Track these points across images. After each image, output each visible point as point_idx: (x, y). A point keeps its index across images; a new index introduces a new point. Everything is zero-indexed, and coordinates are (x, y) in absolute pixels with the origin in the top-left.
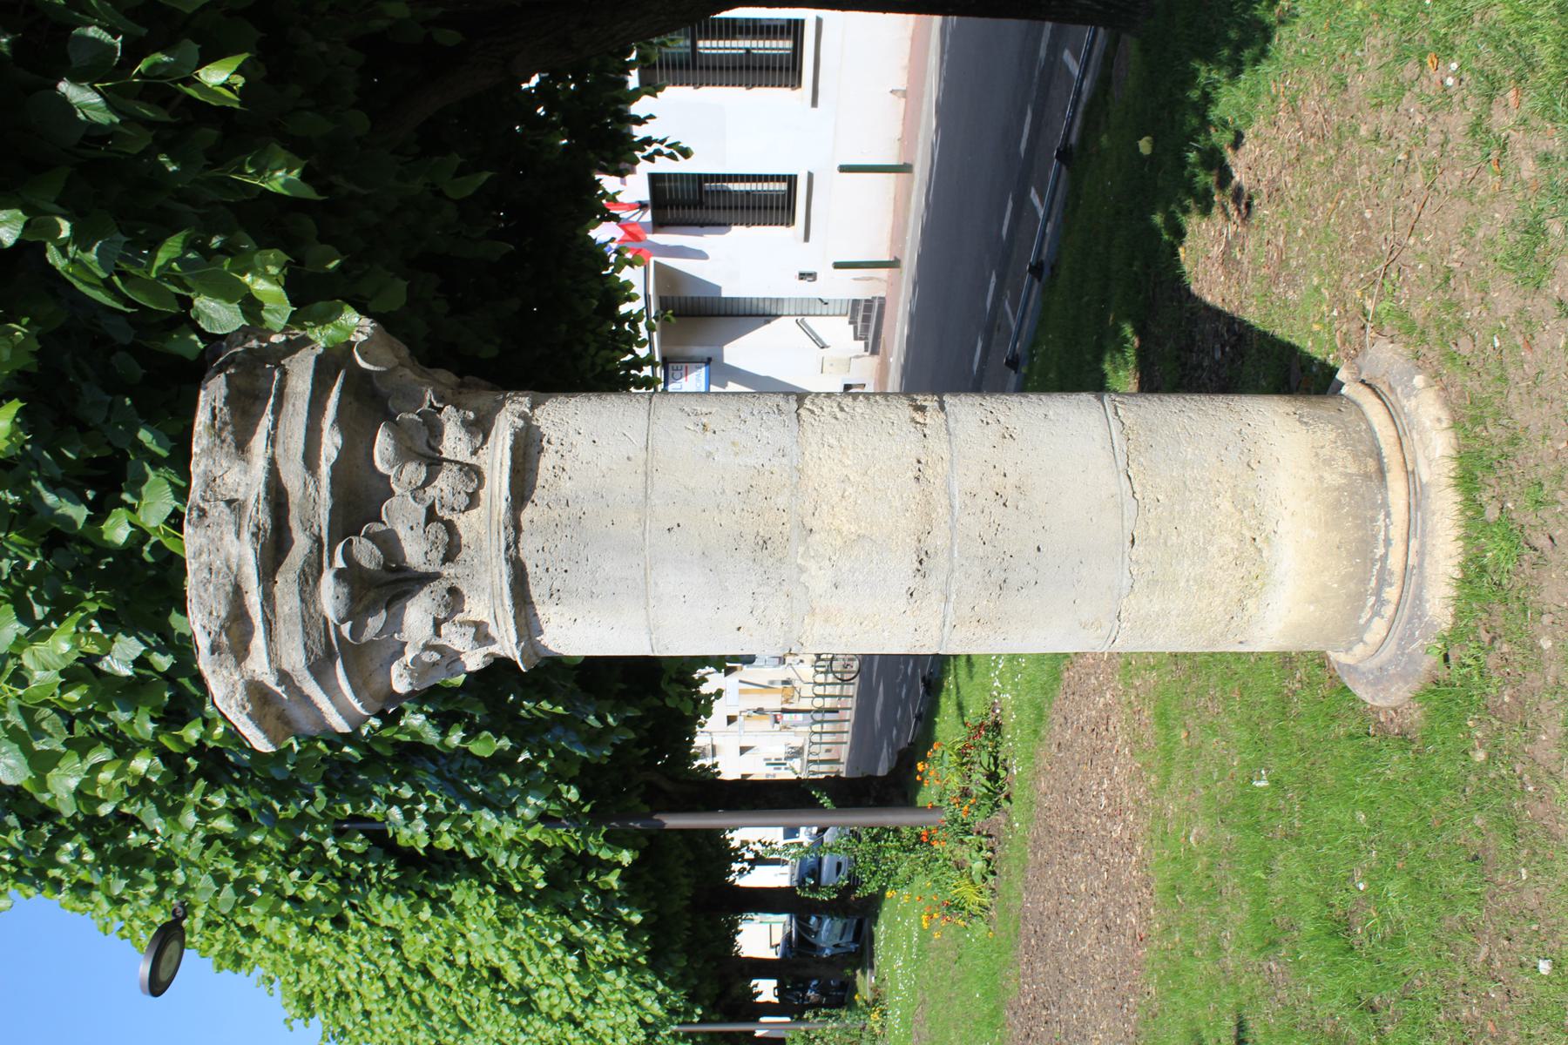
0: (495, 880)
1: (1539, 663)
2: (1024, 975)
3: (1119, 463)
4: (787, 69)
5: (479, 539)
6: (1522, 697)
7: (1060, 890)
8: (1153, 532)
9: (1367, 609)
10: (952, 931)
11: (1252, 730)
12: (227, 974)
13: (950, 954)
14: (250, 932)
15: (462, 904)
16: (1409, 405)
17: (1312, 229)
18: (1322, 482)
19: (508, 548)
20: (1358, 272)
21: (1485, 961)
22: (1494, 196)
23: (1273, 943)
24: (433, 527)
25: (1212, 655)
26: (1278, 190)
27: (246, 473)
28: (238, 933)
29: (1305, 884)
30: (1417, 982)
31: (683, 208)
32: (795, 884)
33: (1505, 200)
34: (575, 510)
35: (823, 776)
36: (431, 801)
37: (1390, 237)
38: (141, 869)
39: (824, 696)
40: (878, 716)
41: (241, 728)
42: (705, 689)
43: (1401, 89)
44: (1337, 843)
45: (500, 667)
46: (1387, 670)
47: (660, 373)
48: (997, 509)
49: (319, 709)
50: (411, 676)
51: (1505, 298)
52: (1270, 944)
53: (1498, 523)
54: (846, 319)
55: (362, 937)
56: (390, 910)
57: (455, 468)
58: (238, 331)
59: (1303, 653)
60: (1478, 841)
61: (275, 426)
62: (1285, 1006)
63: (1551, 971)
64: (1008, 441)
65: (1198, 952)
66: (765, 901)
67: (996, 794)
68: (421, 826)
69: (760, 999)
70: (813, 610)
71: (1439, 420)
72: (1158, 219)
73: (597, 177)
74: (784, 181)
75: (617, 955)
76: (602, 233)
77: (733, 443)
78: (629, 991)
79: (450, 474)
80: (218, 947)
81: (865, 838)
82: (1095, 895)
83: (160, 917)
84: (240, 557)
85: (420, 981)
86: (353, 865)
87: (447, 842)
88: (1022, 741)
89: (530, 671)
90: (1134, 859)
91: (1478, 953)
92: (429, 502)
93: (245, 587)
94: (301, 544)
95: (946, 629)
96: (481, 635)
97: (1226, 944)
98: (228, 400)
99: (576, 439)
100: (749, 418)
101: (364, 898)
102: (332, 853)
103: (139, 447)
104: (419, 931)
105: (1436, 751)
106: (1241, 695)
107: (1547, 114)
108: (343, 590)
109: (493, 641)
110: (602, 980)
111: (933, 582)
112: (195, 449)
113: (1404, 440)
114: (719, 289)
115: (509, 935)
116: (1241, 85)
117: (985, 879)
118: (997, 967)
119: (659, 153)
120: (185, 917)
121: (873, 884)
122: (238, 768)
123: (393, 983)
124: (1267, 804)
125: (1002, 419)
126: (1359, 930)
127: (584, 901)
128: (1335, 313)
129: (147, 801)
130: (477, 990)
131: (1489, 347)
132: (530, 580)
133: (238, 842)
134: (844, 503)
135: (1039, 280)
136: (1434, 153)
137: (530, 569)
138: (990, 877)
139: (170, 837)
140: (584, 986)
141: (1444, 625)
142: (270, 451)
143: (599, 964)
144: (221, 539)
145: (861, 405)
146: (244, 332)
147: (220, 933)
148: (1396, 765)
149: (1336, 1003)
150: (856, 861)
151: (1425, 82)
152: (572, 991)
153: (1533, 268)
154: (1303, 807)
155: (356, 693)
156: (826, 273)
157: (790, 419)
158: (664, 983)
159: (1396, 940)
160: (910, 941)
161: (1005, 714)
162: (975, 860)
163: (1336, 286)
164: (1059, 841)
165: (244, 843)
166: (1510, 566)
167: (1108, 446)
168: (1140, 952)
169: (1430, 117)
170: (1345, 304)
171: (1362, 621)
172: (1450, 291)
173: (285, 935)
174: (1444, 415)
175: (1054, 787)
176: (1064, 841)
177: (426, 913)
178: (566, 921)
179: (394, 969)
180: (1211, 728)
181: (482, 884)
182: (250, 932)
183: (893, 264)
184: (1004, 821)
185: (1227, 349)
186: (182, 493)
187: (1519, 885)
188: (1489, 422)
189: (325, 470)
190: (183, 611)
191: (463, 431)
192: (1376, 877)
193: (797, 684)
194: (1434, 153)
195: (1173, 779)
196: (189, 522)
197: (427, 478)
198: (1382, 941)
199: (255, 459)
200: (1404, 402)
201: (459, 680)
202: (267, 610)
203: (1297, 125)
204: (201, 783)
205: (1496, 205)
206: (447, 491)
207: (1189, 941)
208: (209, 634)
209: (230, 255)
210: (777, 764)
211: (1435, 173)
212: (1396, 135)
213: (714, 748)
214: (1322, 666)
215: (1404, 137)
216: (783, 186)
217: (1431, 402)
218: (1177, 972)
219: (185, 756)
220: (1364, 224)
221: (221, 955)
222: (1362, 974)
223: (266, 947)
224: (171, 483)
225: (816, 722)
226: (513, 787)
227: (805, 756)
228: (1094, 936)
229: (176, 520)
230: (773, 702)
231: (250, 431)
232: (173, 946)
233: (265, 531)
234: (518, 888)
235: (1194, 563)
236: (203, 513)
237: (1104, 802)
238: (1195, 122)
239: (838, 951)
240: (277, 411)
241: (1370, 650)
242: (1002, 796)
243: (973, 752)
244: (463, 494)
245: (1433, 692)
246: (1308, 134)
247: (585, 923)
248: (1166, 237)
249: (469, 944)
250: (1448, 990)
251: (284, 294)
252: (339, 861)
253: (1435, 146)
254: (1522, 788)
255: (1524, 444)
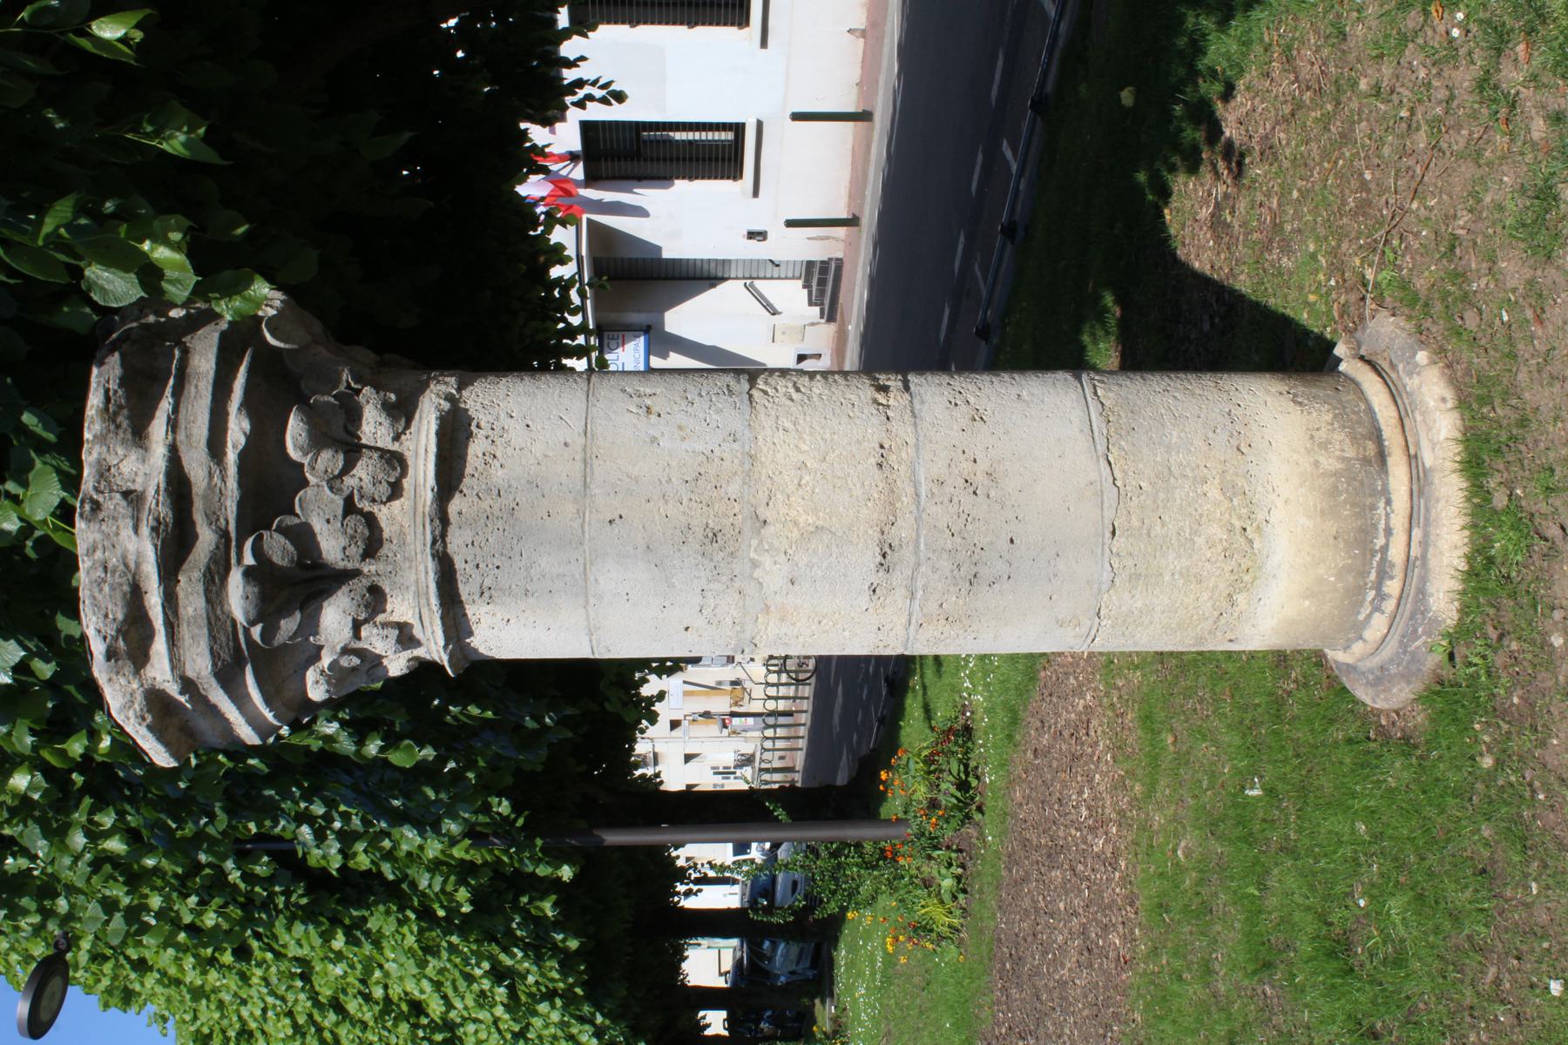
0: (416, 904)
1: (1551, 662)
2: (999, 1003)
3: (1099, 447)
4: (730, 160)
5: (402, 534)
6: (1532, 697)
7: (1037, 910)
8: (1135, 522)
9: (1367, 604)
10: (919, 956)
11: (1244, 735)
12: (115, 1012)
13: (917, 980)
14: (141, 966)
15: (379, 931)
16: (1412, 383)
17: (1308, 191)
18: (1317, 467)
19: (434, 542)
20: (1358, 238)
21: (1493, 982)
22: (1503, 158)
23: (1268, 965)
24: (352, 520)
25: (1200, 653)
26: (1271, 148)
27: (144, 461)
28: (128, 966)
29: (1300, 900)
30: (1421, 1006)
31: (619, 160)
32: (746, 905)
33: (1514, 162)
34: (507, 500)
35: (776, 786)
36: (346, 817)
37: (1391, 201)
38: (20, 898)
39: (776, 698)
40: (836, 719)
41: (140, 741)
42: (646, 691)
43: (1404, 40)
44: (1335, 857)
45: (425, 670)
46: (1388, 670)
47: (593, 340)
48: (967, 499)
49: (227, 720)
50: (328, 683)
51: (1514, 270)
52: (1264, 965)
53: (1507, 511)
54: (800, 283)
55: (267, 969)
56: (299, 939)
57: (376, 455)
58: (134, 304)
59: (1299, 652)
60: (1486, 853)
61: (176, 409)
62: (1280, 1033)
63: (1563, 992)
64: (979, 424)
65: (1185, 975)
66: (713, 924)
67: (967, 805)
68: (333, 847)
69: (708, 1032)
70: (767, 607)
71: (1444, 400)
72: (1142, 177)
73: (523, 126)
74: (730, 130)
75: (551, 985)
76: (532, 188)
77: (680, 428)
78: (563, 1025)
79: (370, 462)
80: (106, 982)
81: (824, 854)
82: (1075, 914)
83: (39, 950)
84: (139, 554)
85: (332, 1017)
86: (257, 889)
87: (363, 861)
88: (995, 747)
89: (459, 676)
90: (1117, 874)
91: (1486, 974)
92: (346, 492)
93: (144, 586)
94: (206, 538)
95: (912, 627)
96: (406, 637)
97: (1217, 967)
98: (123, 382)
99: (508, 423)
100: (697, 399)
101: (270, 925)
102: (235, 876)
103: (24, 430)
104: (331, 961)
105: (1441, 757)
106: (1232, 697)
107: (1559, 70)
108: (253, 590)
109: (418, 644)
110: (535, 1013)
111: (899, 577)
112: (87, 435)
113: (1406, 421)
114: (659, 249)
115: (431, 965)
116: (1232, 32)
117: (955, 898)
118: (969, 994)
119: (589, 97)
120: (68, 949)
121: (833, 904)
122: (130, 786)
123: (301, 1020)
124: (1261, 815)
125: (972, 400)
126: (1359, 950)
127: (514, 926)
128: (1333, 283)
129: (30, 822)
130: (396, 1025)
131: (1497, 321)
132: (459, 577)
133: (130, 866)
134: (800, 492)
135: (1012, 243)
136: (1439, 110)
137: (459, 564)
138: (961, 896)
139: (53, 860)
140: (514, 1020)
141: (1449, 622)
142: (170, 437)
143: (531, 995)
144: (117, 534)
145: (819, 385)
146: (141, 306)
147: (108, 967)
148: (1397, 772)
149: (1335, 1029)
150: (813, 880)
151: (1430, 33)
152: (502, 1026)
153: (1542, 238)
154: (1299, 817)
155: (268, 701)
156: (777, 231)
157: (742, 401)
158: (603, 1015)
159: (1399, 961)
160: (873, 967)
161: (977, 717)
162: (945, 877)
163: (1333, 253)
164: (1035, 856)
165: (136, 867)
166: (1519, 558)
167: (1087, 429)
168: (1124, 976)
169: (1434, 71)
170: (1343, 273)
171: (1361, 617)
172: (1456, 260)
173: (181, 969)
174: (1449, 395)
175: (1029, 797)
176: (1041, 856)
177: (339, 942)
178: (495, 949)
179: (303, 1004)
180: (1199, 732)
181: (401, 909)
182: (141, 966)
183: (852, 222)
184: (975, 834)
185: (1217, 320)
186: (72, 482)
187: (1529, 899)
188: (1497, 401)
189: (231, 457)
190: (75, 614)
191: (384, 415)
192: (1377, 895)
193: (747, 685)
194: (1439, 110)
195: (1159, 788)
196: (81, 515)
197: (344, 466)
198: (1384, 962)
199: (154, 446)
200: (1406, 380)
201: (379, 685)
202: (169, 613)
203: (1292, 77)
204: (87, 801)
205: (1505, 168)
206: (367, 479)
207: (1177, 964)
208: (105, 638)
209: (126, 221)
210: (726, 773)
211: (1440, 131)
212: (1398, 90)
213: (656, 756)
214: (1319, 665)
215: (1406, 93)
216: (730, 136)
217: (1435, 380)
218: (1164, 997)
219: (71, 771)
220: (1364, 186)
221: (109, 991)
222: (1363, 997)
223: (159, 982)
224: (59, 471)
225: (768, 726)
226: (438, 801)
227: (757, 764)
228: (1074, 959)
229: (65, 513)
230: (721, 705)
231: (150, 416)
232: (56, 982)
233: (167, 525)
234: (441, 913)
235: (1179, 556)
236: (96, 507)
237: (1085, 813)
238: (1182, 71)
239: (795, 978)
240: (178, 393)
241: (1370, 648)
242: (974, 807)
243: (941, 759)
244: (384, 483)
245: (1438, 693)
246: (1303, 86)
247: (515, 950)
248: (1150, 197)
249: (387, 974)
250: (1454, 1013)
251: (187, 262)
252: (242, 886)
253: (1440, 103)
254: (1532, 797)
255: (1534, 426)
